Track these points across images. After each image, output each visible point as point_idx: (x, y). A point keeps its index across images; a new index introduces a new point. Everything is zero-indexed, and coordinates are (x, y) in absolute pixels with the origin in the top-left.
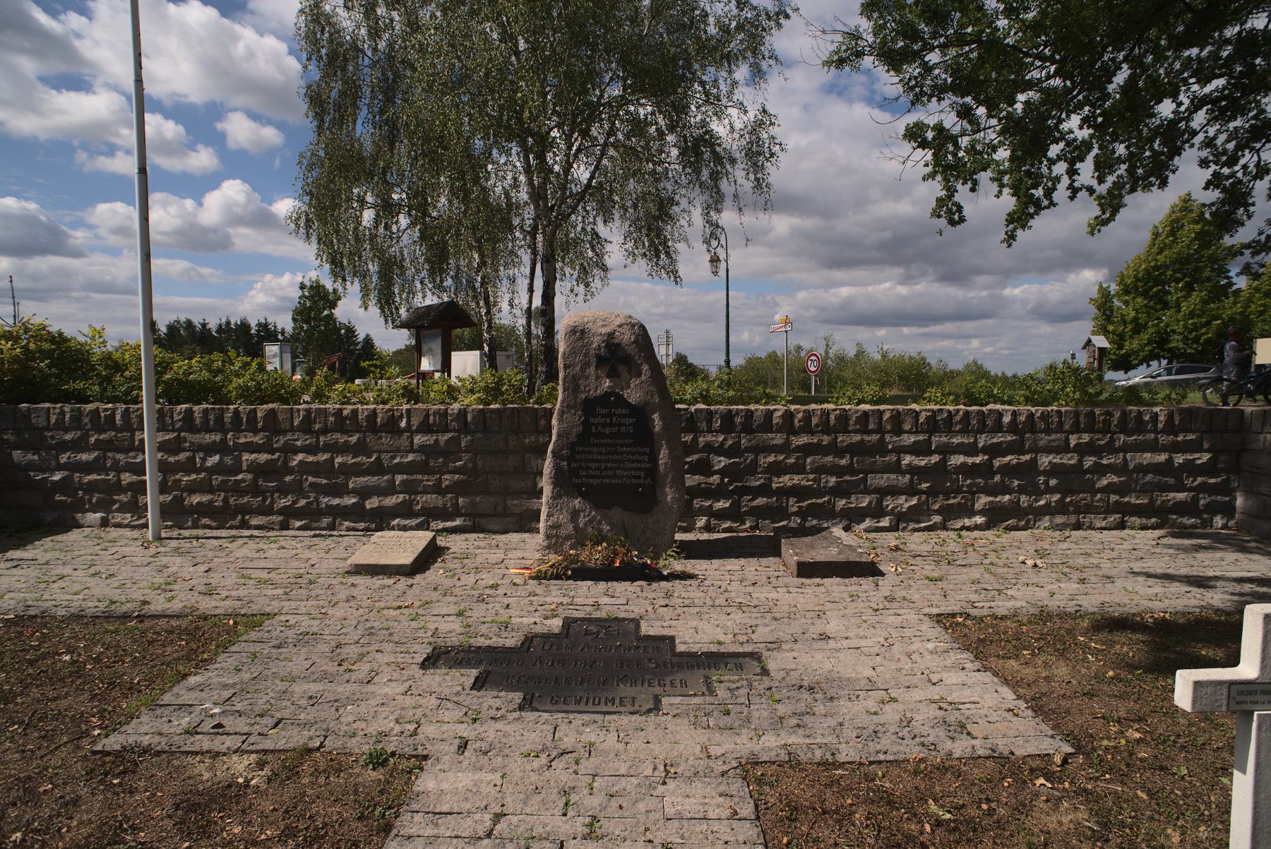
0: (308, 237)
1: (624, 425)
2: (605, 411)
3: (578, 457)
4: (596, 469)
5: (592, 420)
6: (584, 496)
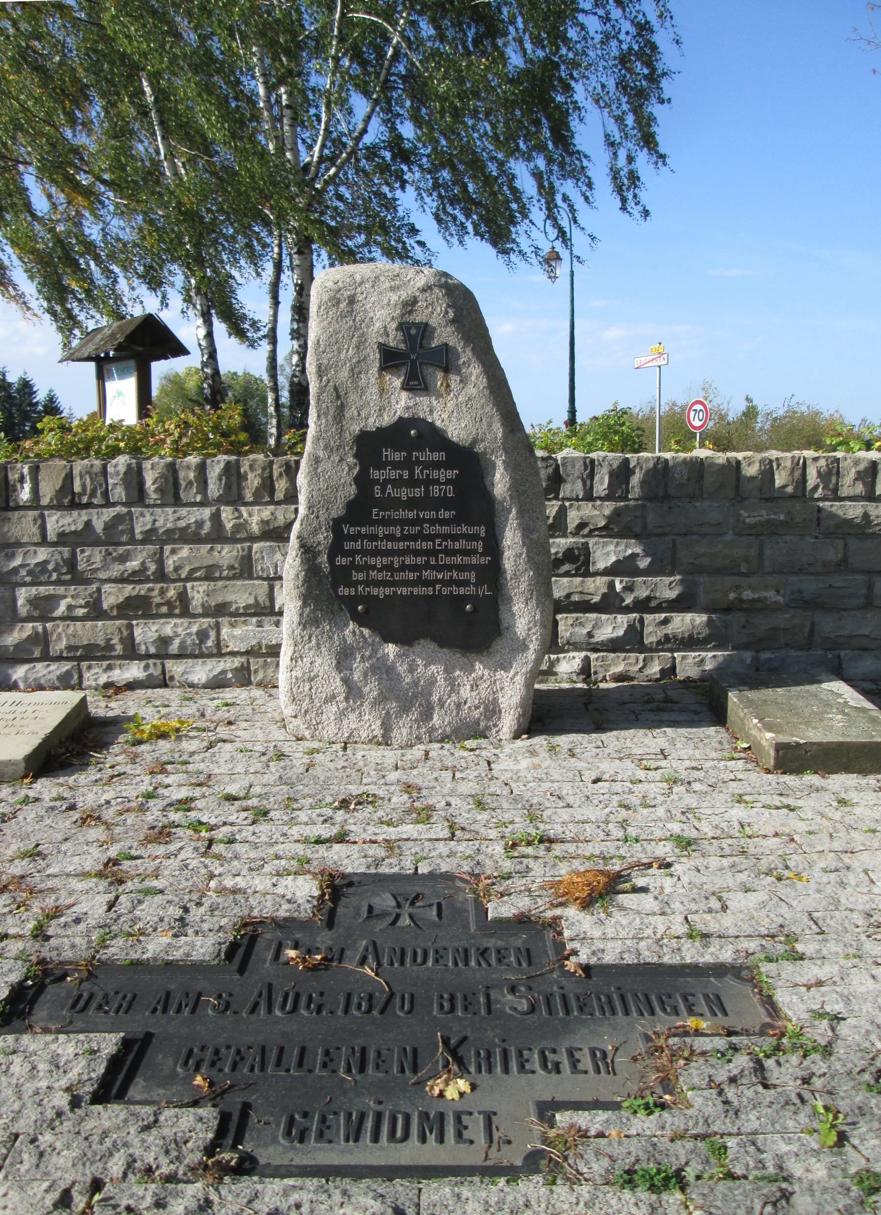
0: (653, 1013)
1: (437, 482)
2: (398, 456)
3: (348, 546)
4: (385, 568)
5: (375, 474)
6: (361, 620)
